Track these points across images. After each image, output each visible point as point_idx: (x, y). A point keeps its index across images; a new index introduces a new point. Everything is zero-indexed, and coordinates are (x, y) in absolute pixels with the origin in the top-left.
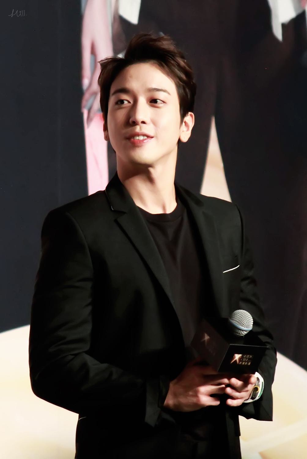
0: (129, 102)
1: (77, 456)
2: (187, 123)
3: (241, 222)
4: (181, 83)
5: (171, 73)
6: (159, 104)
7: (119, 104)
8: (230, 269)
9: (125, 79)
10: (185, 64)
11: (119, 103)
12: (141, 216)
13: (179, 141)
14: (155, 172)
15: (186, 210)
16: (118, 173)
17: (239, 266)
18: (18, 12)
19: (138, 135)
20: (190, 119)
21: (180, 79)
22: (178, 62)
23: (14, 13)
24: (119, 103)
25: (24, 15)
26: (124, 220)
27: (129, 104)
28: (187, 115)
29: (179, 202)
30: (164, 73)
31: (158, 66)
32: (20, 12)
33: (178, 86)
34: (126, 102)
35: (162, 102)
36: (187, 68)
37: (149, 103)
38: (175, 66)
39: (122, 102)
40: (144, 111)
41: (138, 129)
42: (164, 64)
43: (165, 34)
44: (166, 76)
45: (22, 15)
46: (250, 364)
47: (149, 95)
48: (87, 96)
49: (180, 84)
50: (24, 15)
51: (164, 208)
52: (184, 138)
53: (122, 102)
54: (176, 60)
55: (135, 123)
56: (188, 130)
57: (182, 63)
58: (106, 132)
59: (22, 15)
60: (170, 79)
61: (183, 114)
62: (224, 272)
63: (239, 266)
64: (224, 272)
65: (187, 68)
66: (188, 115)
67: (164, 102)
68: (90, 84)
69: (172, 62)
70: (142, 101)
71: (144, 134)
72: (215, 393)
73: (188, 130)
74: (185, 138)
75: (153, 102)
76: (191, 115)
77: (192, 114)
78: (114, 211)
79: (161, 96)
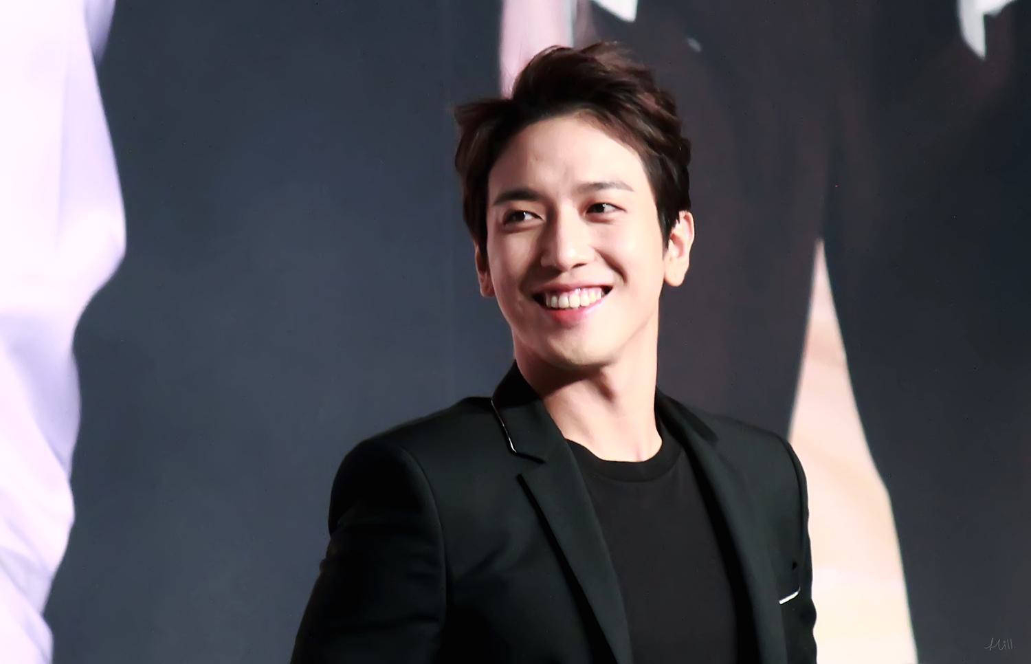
0: (535, 216)
1: (78, 606)
2: (679, 238)
4: (654, 153)
5: (628, 134)
6: (608, 212)
9: (520, 165)
10: (590, 56)
11: (514, 218)
12: (566, 442)
13: (666, 285)
14: (616, 377)
15: (683, 455)
16: (519, 366)
17: (796, 594)
18: (1001, 642)
19: (567, 289)
20: (684, 229)
21: (651, 143)
22: (641, 104)
23: (995, 643)
24: (514, 218)
26: (539, 480)
27: (538, 222)
29: (666, 433)
31: (595, 119)
32: (1004, 642)
33: (648, 161)
34: (528, 217)
35: (614, 208)
36: (665, 113)
37: (584, 214)
38: (638, 117)
39: (520, 215)
40: (576, 241)
41: (564, 279)
42: (611, 116)
44: (618, 142)
45: (1007, 648)
47: (582, 198)
53: (520, 215)
54: (637, 101)
55: (557, 270)
57: (650, 102)
58: (486, 274)
61: (667, 221)
62: (782, 602)
63: (796, 594)
64: (782, 602)
65: (665, 113)
67: (618, 208)
69: (628, 106)
70: (569, 213)
71: (581, 285)
73: (681, 254)
74: (677, 279)
75: (593, 210)
76: (686, 218)
77: (690, 215)
79: (610, 195)
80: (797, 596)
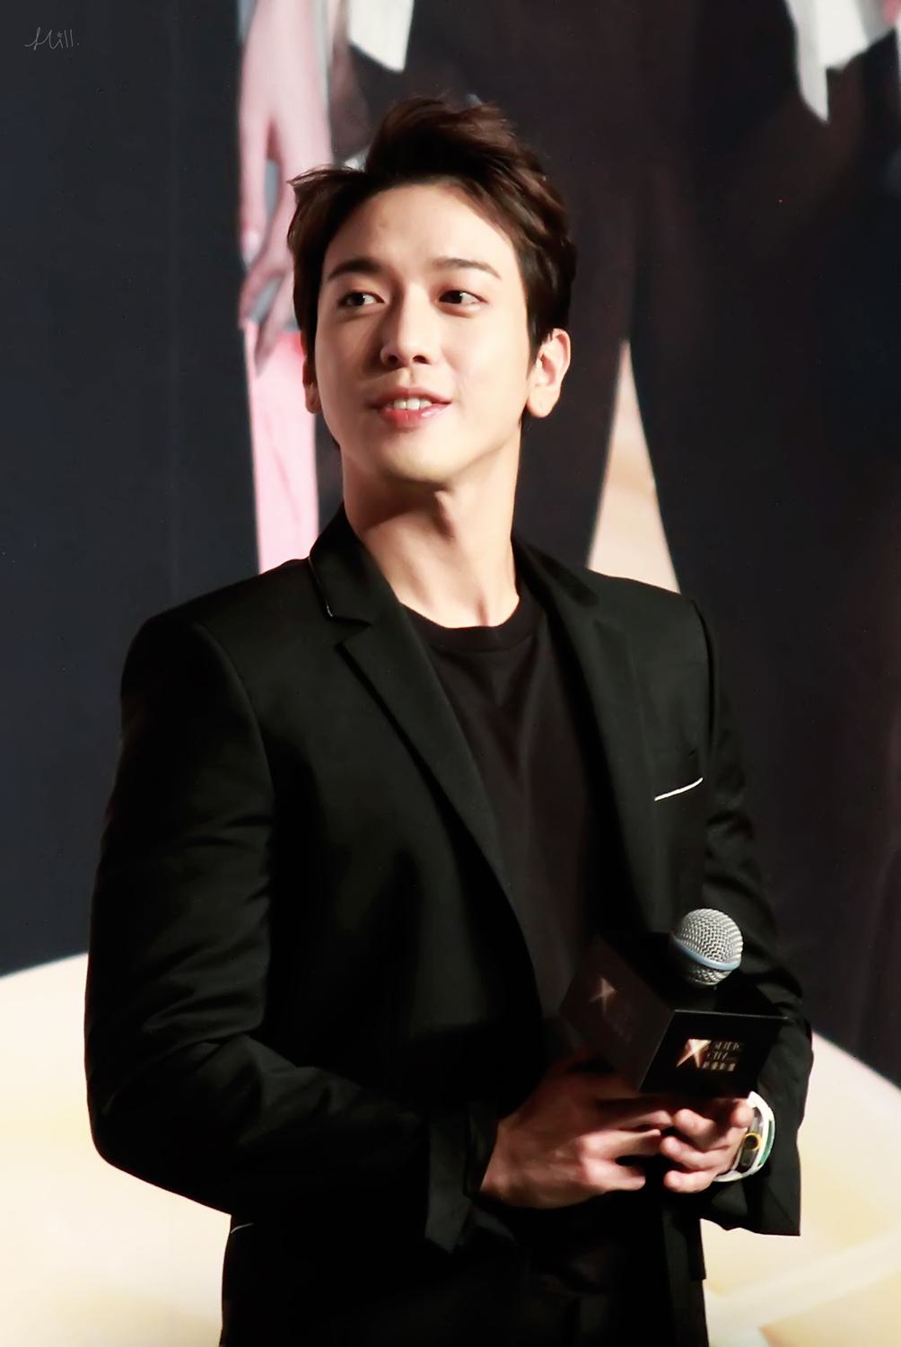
0: (379, 300)
2: (549, 362)
3: (706, 652)
4: (531, 244)
5: (502, 216)
6: (467, 305)
7: (349, 306)
8: (675, 789)
9: (366, 233)
11: (349, 302)
12: (414, 633)
13: (527, 414)
14: (455, 506)
15: (544, 617)
16: (346, 507)
17: (701, 780)
18: (54, 35)
19: (405, 396)
20: (557, 350)
21: (529, 232)
22: (523, 182)
24: (349, 302)
25: (70, 44)
26: (363, 647)
27: (380, 307)
28: (549, 337)
29: (526, 592)
30: (480, 215)
31: (463, 194)
32: (59, 35)
33: (522, 253)
34: (369, 300)
35: (476, 300)
36: (549, 199)
37: (436, 301)
38: (512, 194)
39: (358, 298)
40: (422, 327)
41: (404, 379)
42: (481, 189)
43: (484, 98)
44: (488, 223)
45: (65, 45)
46: (735, 1068)
47: (438, 278)
48: (254, 281)
49: (527, 247)
50: (70, 44)
51: (481, 610)
52: (541, 405)
53: (358, 298)
54: (517, 177)
55: (396, 362)
56: (552, 381)
57: (534, 184)
58: (311, 386)
59: (65, 45)
60: (498, 232)
61: (538, 336)
62: (657, 799)
63: (701, 780)
64: (657, 799)
65: (549, 199)
66: (551, 339)
67: (481, 299)
68: (265, 247)
69: (506, 182)
70: (418, 298)
71: (422, 392)
72: (632, 1153)
73: (552, 381)
74: (544, 405)
75: (449, 298)
76: (561, 338)
77: (565, 334)
78: (336, 620)
79: (471, 281)
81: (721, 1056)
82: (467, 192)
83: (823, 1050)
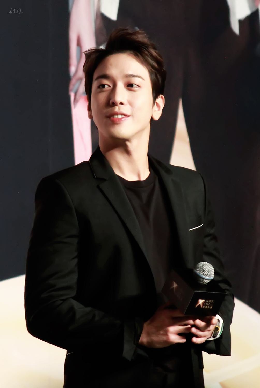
0: (109, 86)
2: (159, 104)
3: (204, 188)
4: (153, 70)
5: (145, 62)
6: (135, 88)
7: (101, 88)
8: (195, 227)
9: (106, 67)
11: (101, 87)
12: (119, 182)
13: (152, 119)
14: (131, 146)
16: (100, 146)
17: (202, 225)
18: (16, 10)
19: (117, 114)
20: (161, 101)
21: (153, 67)
22: (151, 53)
24: (101, 87)
25: (20, 13)
26: (105, 186)
27: (110, 88)
28: (158, 97)
30: (139, 62)
31: (134, 56)
32: (17, 10)
33: (151, 73)
34: (106, 86)
35: (137, 86)
36: (159, 57)
37: (126, 87)
38: (148, 56)
39: (103, 86)
40: (122, 94)
41: (117, 109)
42: (139, 54)
43: (140, 28)
44: (141, 64)
45: (19, 13)
46: (212, 308)
47: (126, 80)
49: (152, 71)
50: (20, 13)
52: (156, 117)
53: (103, 86)
54: (149, 51)
55: (114, 104)
56: (159, 110)
57: (154, 53)
58: (90, 111)
59: (19, 13)
60: (144, 67)
61: (155, 97)
62: (190, 230)
63: (202, 225)
64: (190, 230)
65: (159, 57)
66: (159, 98)
67: (139, 86)
68: (77, 71)
69: (146, 52)
70: (121, 86)
71: (122, 113)
72: (182, 332)
73: (159, 110)
74: (157, 117)
75: (130, 86)
76: (162, 97)
77: (163, 96)
78: (97, 178)
79: (136, 81)
80: (190, 229)
81: (208, 304)
82: (135, 55)
83: (237, 303)
